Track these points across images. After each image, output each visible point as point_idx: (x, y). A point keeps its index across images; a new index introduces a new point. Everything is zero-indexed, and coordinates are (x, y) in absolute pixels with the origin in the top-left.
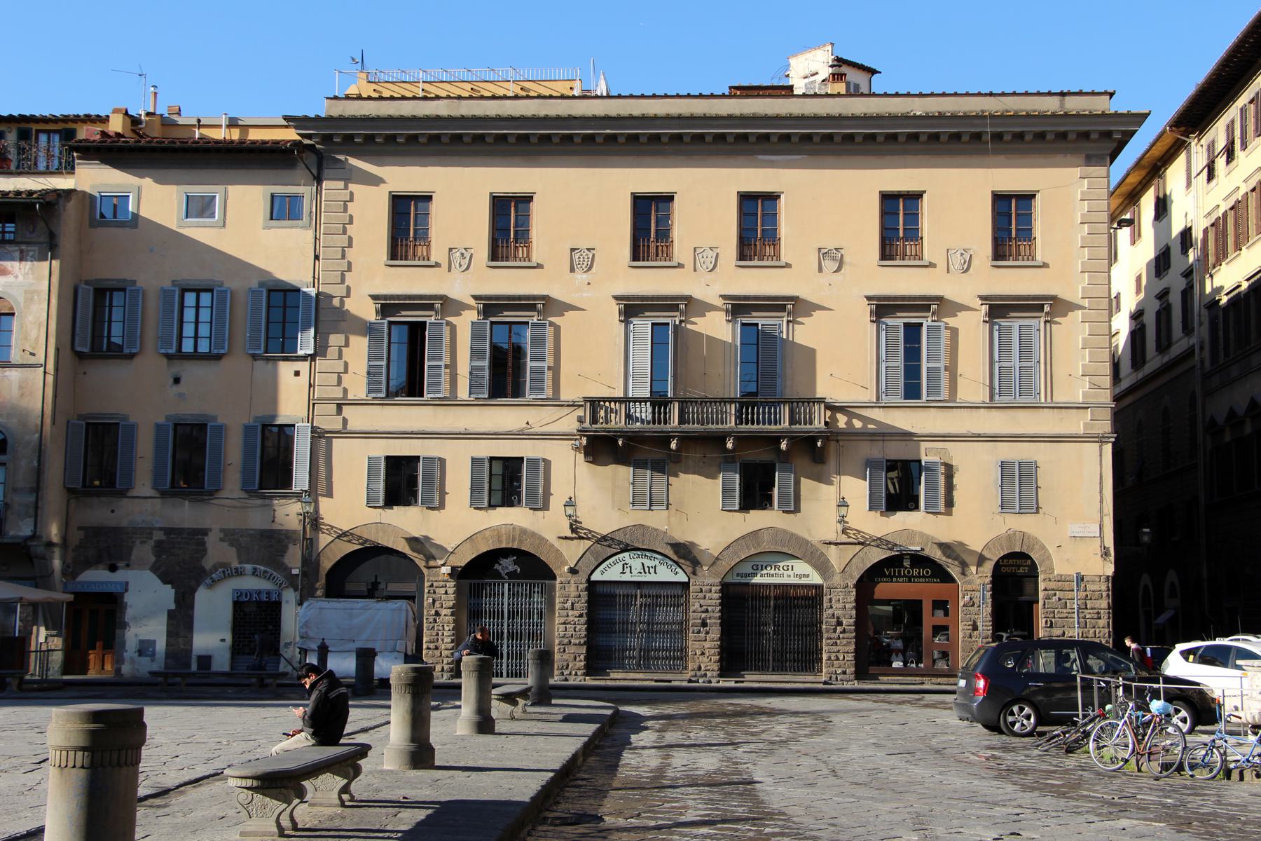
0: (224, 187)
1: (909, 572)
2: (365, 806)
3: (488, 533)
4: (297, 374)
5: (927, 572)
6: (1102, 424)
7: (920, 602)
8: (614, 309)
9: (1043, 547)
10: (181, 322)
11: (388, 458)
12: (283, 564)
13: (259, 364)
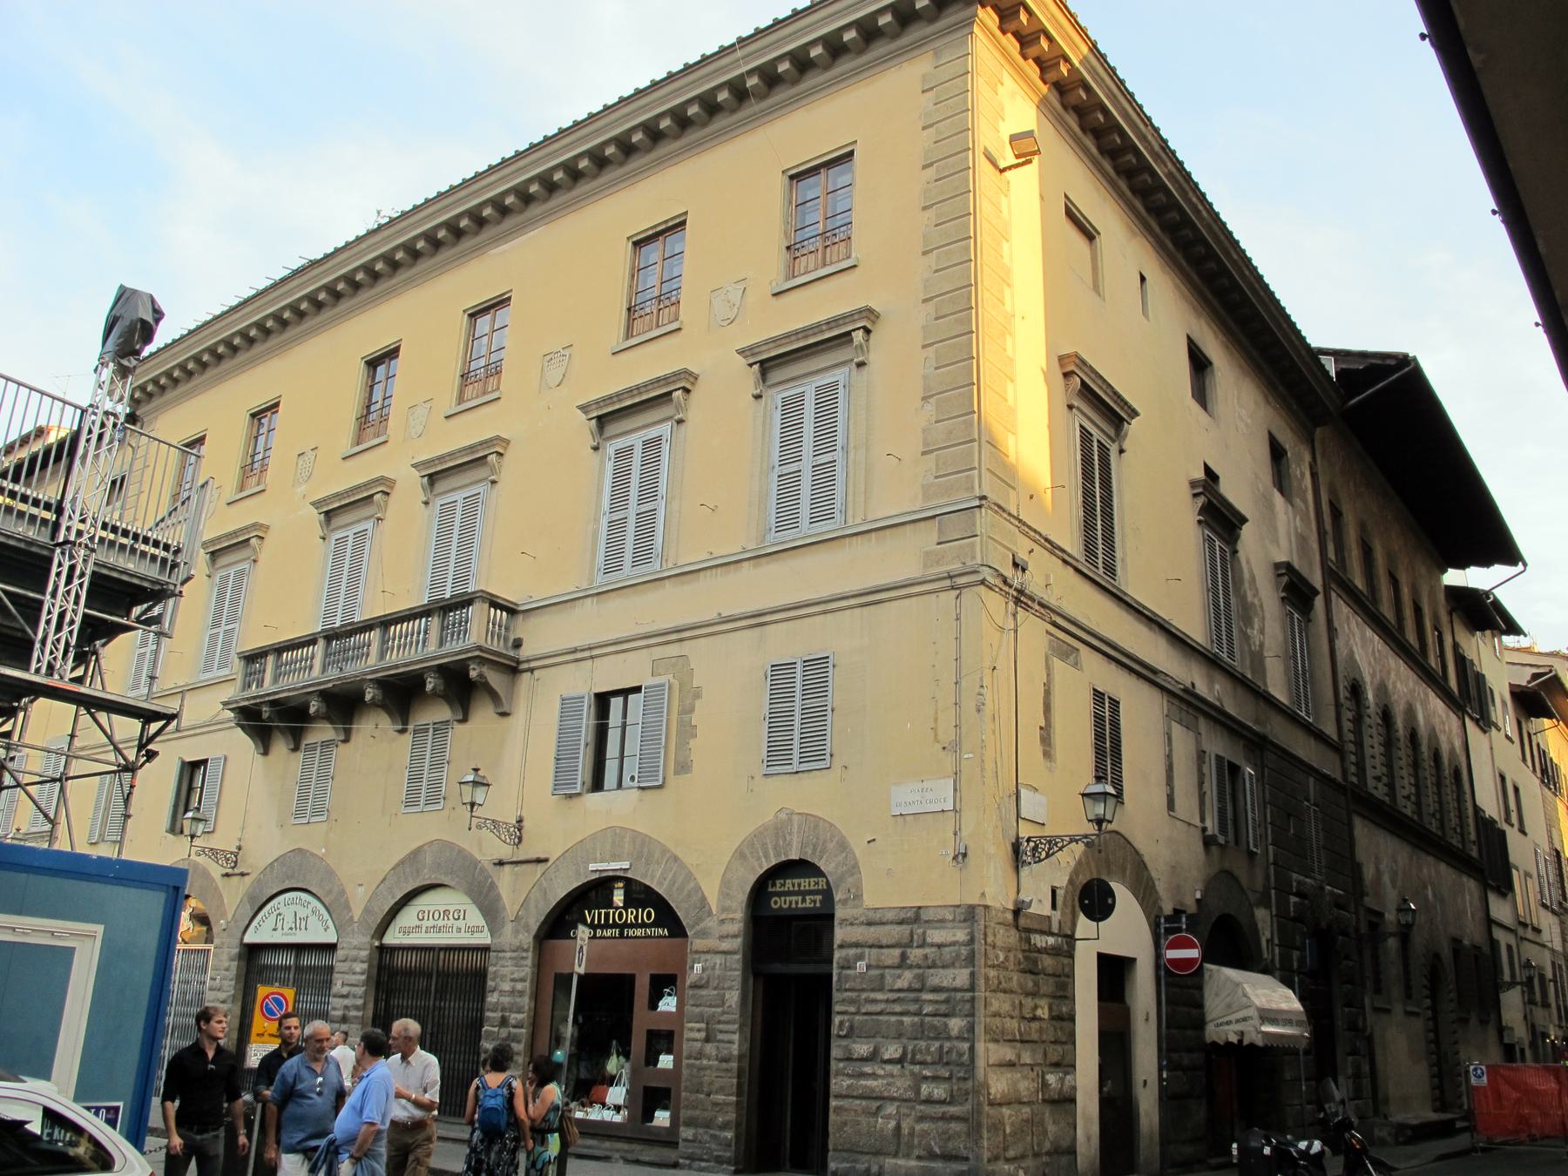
0: (685, 1042)
1: (621, 915)
2: (215, 731)
6: (961, 547)
8: (315, 516)
9: (843, 846)
10: (647, 937)
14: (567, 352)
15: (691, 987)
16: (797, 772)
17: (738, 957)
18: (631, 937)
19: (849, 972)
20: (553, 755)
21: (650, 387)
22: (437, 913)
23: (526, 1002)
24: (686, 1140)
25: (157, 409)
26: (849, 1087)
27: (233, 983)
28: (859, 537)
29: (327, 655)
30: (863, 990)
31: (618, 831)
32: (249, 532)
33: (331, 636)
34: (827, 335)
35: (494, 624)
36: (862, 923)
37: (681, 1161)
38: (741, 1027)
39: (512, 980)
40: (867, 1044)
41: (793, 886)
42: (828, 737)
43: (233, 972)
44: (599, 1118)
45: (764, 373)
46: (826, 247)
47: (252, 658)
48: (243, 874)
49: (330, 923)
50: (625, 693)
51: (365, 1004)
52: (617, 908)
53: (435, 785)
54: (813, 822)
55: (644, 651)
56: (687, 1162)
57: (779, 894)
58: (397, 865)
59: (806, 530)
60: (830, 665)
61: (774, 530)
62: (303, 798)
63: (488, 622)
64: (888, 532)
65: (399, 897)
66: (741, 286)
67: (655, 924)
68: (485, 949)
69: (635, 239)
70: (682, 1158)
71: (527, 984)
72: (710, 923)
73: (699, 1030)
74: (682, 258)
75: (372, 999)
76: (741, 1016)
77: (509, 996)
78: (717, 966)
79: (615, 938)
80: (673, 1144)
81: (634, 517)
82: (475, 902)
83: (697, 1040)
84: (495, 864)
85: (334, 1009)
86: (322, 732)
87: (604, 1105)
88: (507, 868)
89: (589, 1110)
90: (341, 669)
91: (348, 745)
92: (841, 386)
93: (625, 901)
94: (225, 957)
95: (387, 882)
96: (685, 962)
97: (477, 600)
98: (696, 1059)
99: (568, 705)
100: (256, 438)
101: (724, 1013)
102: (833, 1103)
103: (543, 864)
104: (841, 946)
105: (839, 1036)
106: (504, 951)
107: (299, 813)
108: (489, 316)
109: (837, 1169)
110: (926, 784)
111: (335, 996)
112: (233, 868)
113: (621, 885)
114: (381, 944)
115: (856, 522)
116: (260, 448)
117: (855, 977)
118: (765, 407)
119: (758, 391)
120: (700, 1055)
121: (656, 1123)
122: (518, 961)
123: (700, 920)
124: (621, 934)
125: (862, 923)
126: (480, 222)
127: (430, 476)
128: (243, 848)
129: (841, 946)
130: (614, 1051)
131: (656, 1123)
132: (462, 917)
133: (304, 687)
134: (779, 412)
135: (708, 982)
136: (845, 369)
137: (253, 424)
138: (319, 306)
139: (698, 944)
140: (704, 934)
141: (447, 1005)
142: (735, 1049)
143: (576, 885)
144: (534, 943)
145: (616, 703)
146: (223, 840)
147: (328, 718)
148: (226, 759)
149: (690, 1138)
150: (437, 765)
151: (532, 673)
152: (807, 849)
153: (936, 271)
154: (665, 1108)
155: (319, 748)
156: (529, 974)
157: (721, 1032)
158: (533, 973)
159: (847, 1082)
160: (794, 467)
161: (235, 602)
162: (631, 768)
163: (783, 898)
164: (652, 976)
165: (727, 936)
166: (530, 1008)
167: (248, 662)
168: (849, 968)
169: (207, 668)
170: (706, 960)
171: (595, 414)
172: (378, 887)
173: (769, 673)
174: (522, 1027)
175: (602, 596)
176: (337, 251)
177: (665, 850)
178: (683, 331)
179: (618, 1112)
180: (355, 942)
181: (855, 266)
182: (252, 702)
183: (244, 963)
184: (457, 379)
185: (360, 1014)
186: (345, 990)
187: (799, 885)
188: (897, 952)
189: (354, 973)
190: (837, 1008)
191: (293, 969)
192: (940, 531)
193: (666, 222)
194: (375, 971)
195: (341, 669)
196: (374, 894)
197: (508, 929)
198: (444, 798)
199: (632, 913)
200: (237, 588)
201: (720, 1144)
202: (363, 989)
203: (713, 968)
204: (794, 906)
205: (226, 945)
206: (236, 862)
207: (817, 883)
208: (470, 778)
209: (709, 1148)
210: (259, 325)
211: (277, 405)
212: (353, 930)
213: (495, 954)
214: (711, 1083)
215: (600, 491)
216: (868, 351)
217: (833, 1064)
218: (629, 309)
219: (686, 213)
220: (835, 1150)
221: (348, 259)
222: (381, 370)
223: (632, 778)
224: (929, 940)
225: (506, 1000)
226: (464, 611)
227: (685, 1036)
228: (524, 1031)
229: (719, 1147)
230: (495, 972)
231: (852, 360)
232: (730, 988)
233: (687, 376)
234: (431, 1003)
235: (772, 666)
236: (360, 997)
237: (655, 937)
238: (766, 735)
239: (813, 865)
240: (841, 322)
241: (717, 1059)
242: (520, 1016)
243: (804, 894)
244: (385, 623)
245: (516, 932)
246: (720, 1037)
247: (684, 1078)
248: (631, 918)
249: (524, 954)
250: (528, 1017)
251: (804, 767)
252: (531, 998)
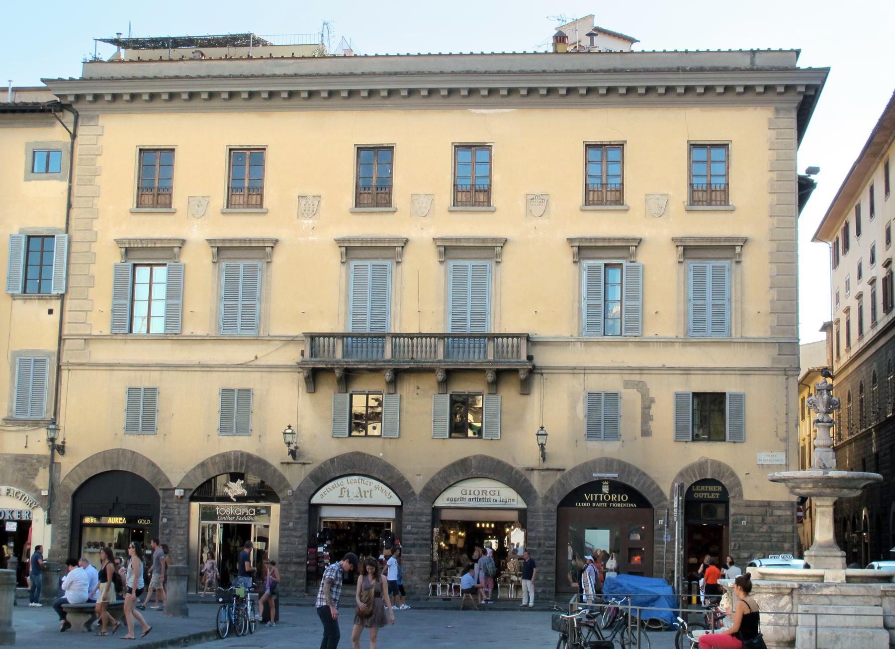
1: (607, 497)
3: (217, 459)
4: (50, 312)
9: (733, 474)
11: (696, 395)
12: (34, 486)
13: (18, 303)
19: (737, 525)
34: (722, 244)
52: (605, 494)
54: (719, 465)
57: (698, 492)
110: (773, 453)
123: (659, 502)
124: (608, 506)
136: (729, 261)
171: (577, 244)
177: (638, 470)
188: (760, 518)
192: (780, 350)
199: (614, 496)
204: (705, 497)
224: (775, 514)
243: (711, 492)
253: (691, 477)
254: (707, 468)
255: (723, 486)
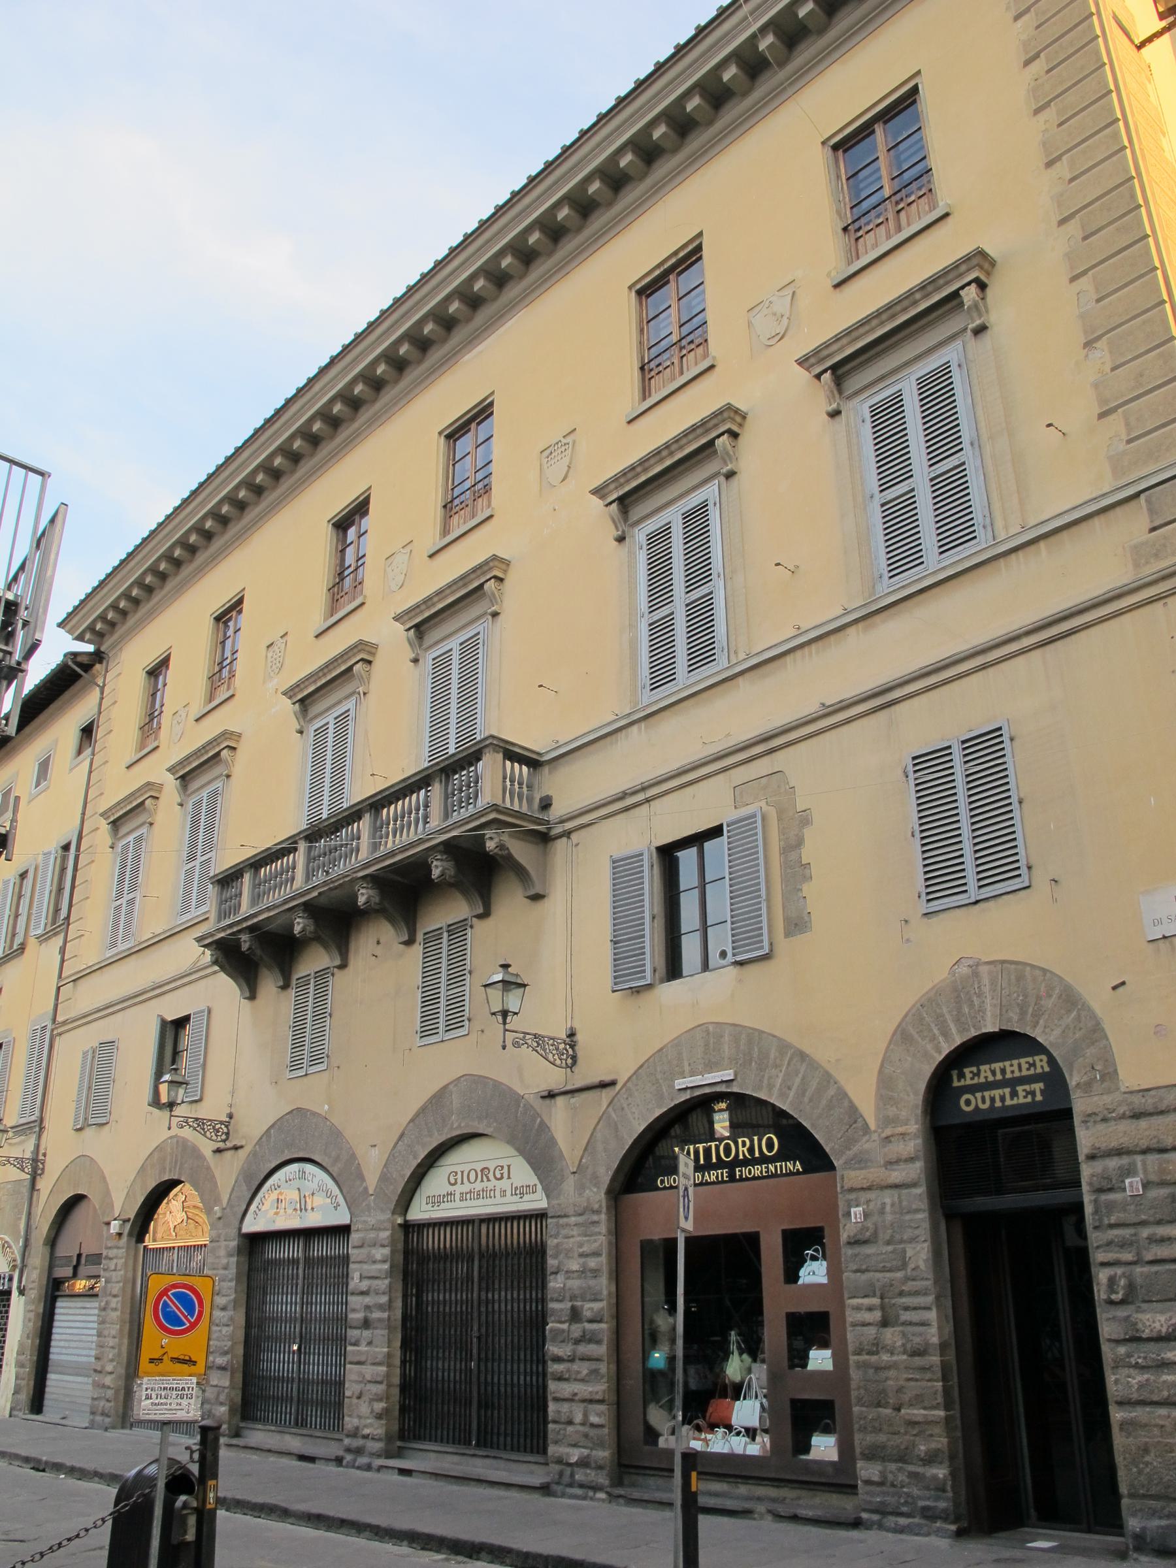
0: (849, 1329)
5: (770, 1146)
7: (752, 1240)
8: (288, 707)
9: (1071, 1000)
14: (569, 440)
15: (849, 1243)
16: (977, 902)
17: (921, 1190)
18: (747, 1179)
19: (1112, 1196)
20: (608, 934)
21: (684, 441)
22: (473, 1172)
23: (604, 1284)
24: (868, 1482)
25: (122, 638)
26: (1141, 1386)
27: (233, 1284)
28: (1020, 553)
29: (310, 859)
30: (1143, 1223)
31: (711, 1028)
32: (218, 744)
33: (313, 834)
35: (512, 781)
36: (1123, 1117)
37: (864, 1515)
38: (938, 1298)
39: (581, 1255)
40: (1162, 1312)
41: (994, 1073)
42: (1020, 842)
43: (233, 1271)
44: (726, 1451)
45: (839, 381)
46: (898, 212)
47: (228, 880)
48: (236, 1148)
49: (341, 1199)
50: (698, 839)
51: (390, 1301)
52: (721, 1140)
53: (456, 1005)
55: (721, 776)
56: (875, 1517)
57: (972, 1089)
58: (417, 1115)
59: (934, 562)
60: (1006, 738)
61: (886, 575)
62: (297, 1045)
63: (505, 778)
64: (1065, 535)
65: (422, 1156)
66: (788, 292)
67: (782, 1156)
68: (541, 1216)
69: (638, 286)
70: (864, 1510)
71: (603, 1259)
72: (866, 1144)
73: (870, 1309)
74: (704, 292)
75: (399, 1295)
76: (935, 1283)
77: (579, 1278)
78: (888, 1208)
79: (723, 1182)
80: (849, 1488)
81: (684, 609)
82: (521, 1152)
83: (869, 1324)
84: (543, 1097)
85: (354, 1310)
86: (315, 961)
87: (729, 1427)
88: (560, 1101)
89: (709, 1436)
90: (327, 872)
91: (346, 970)
92: (954, 368)
93: (734, 1126)
94: (222, 1253)
95: (405, 1139)
96: (835, 1206)
97: (487, 750)
98: (870, 1353)
99: (623, 868)
100: (223, 643)
101: (907, 1279)
102: (1117, 1415)
103: (608, 1090)
104: (1092, 1157)
105: (1111, 1302)
106: (566, 1216)
107: (295, 1065)
108: (469, 435)
109: (1144, 1529)
111: (352, 1294)
112: (224, 1141)
113: (723, 1105)
114: (406, 1221)
115: (1009, 531)
116: (228, 653)
117: (1124, 1207)
118: (848, 424)
119: (834, 406)
120: (876, 1347)
121: (813, 1455)
122: (587, 1228)
123: (850, 1142)
125: (1123, 1117)
126: (448, 324)
127: (417, 627)
128: (235, 1116)
129: (1092, 1157)
130: (733, 1347)
131: (813, 1455)
132: (506, 1175)
133: (285, 902)
134: (868, 425)
135: (876, 1233)
136: (958, 344)
137: (218, 630)
138: (276, 475)
139: (849, 1176)
140: (861, 1161)
141: (496, 1297)
142: (933, 1336)
143: (658, 1112)
144: (608, 1200)
145: (687, 858)
146: (213, 1108)
147: (317, 939)
148: (209, 1012)
149: (876, 1479)
150: (457, 977)
151: (569, 838)
152: (1011, 1014)
153: (1072, 180)
154: (827, 1430)
155: (312, 981)
156: (605, 1244)
157: (906, 1309)
158: (610, 1243)
159: (1139, 1378)
160: (891, 494)
161: (210, 828)
162: (720, 939)
163: (979, 1095)
164: (784, 1232)
165: (898, 1162)
166: (610, 1294)
167: (223, 887)
168: (1111, 1190)
169: (185, 909)
170: (868, 1202)
171: (615, 496)
172: (395, 1147)
173: (911, 769)
174: (600, 1321)
175: (652, 720)
176: (289, 402)
177: (784, 1046)
178: (717, 369)
179: (753, 1439)
180: (372, 1221)
181: (947, 215)
182: (229, 931)
183: (244, 1259)
184: (439, 511)
185: (385, 1315)
186: (364, 1286)
187: (1003, 1071)
189: (374, 1262)
190: (1098, 1256)
191: (302, 1261)
192: (1152, 511)
193: (676, 253)
194: (400, 1258)
195: (327, 872)
196: (392, 1157)
197: (569, 1185)
198: (469, 1020)
199: (744, 1144)
200: (212, 811)
201: (927, 1488)
202: (387, 1282)
203: (882, 1212)
204: (998, 1104)
205: (222, 1238)
206: (227, 1134)
207: (1033, 1065)
208: (499, 977)
209: (908, 1495)
210: (215, 514)
211: (240, 601)
212: (368, 1205)
213: (554, 1220)
214: (900, 1390)
215: (632, 591)
216: (987, 311)
217: (1106, 1349)
218: (642, 368)
219: (700, 234)
220: (1132, 1496)
221: (303, 407)
222: (352, 533)
223: (723, 954)
225: (575, 1284)
226: (472, 769)
227: (849, 1319)
228: (604, 1326)
229: (927, 1493)
230: (558, 1245)
231: (965, 329)
232: (912, 1240)
233: (364, 647)
234: (475, 1295)
235: (914, 758)
236: (384, 1293)
237: (782, 1175)
238: (920, 856)
239: (1025, 1035)
240: (941, 281)
241: (904, 1352)
242: (597, 1306)
243: (1013, 1083)
244: (377, 804)
245: (581, 1188)
246: (906, 1316)
247: (853, 1385)
248: (743, 1151)
249: (595, 1218)
250: (609, 1303)
251: (987, 892)
252: (610, 1279)
253: (933, 1038)
254: (980, 995)
255: (1052, 1061)
